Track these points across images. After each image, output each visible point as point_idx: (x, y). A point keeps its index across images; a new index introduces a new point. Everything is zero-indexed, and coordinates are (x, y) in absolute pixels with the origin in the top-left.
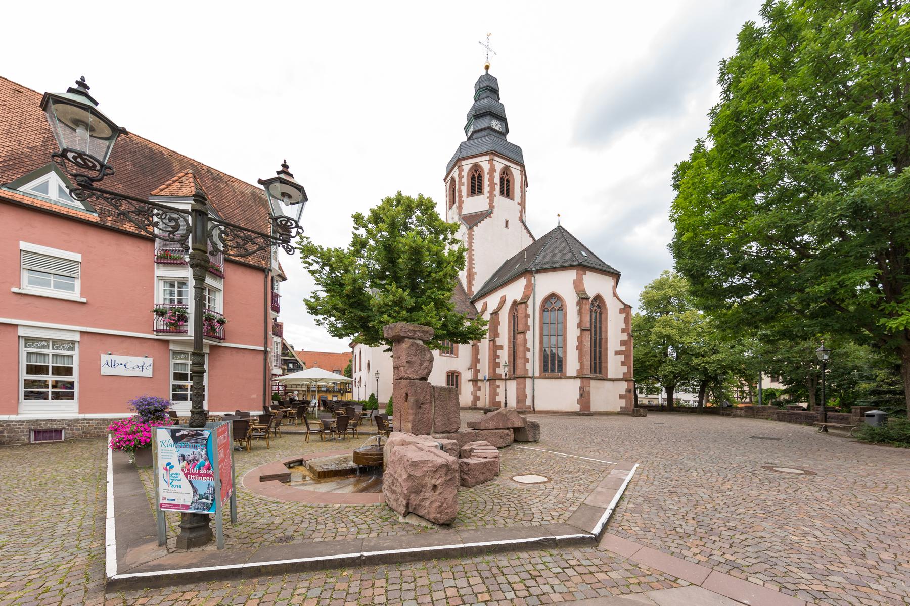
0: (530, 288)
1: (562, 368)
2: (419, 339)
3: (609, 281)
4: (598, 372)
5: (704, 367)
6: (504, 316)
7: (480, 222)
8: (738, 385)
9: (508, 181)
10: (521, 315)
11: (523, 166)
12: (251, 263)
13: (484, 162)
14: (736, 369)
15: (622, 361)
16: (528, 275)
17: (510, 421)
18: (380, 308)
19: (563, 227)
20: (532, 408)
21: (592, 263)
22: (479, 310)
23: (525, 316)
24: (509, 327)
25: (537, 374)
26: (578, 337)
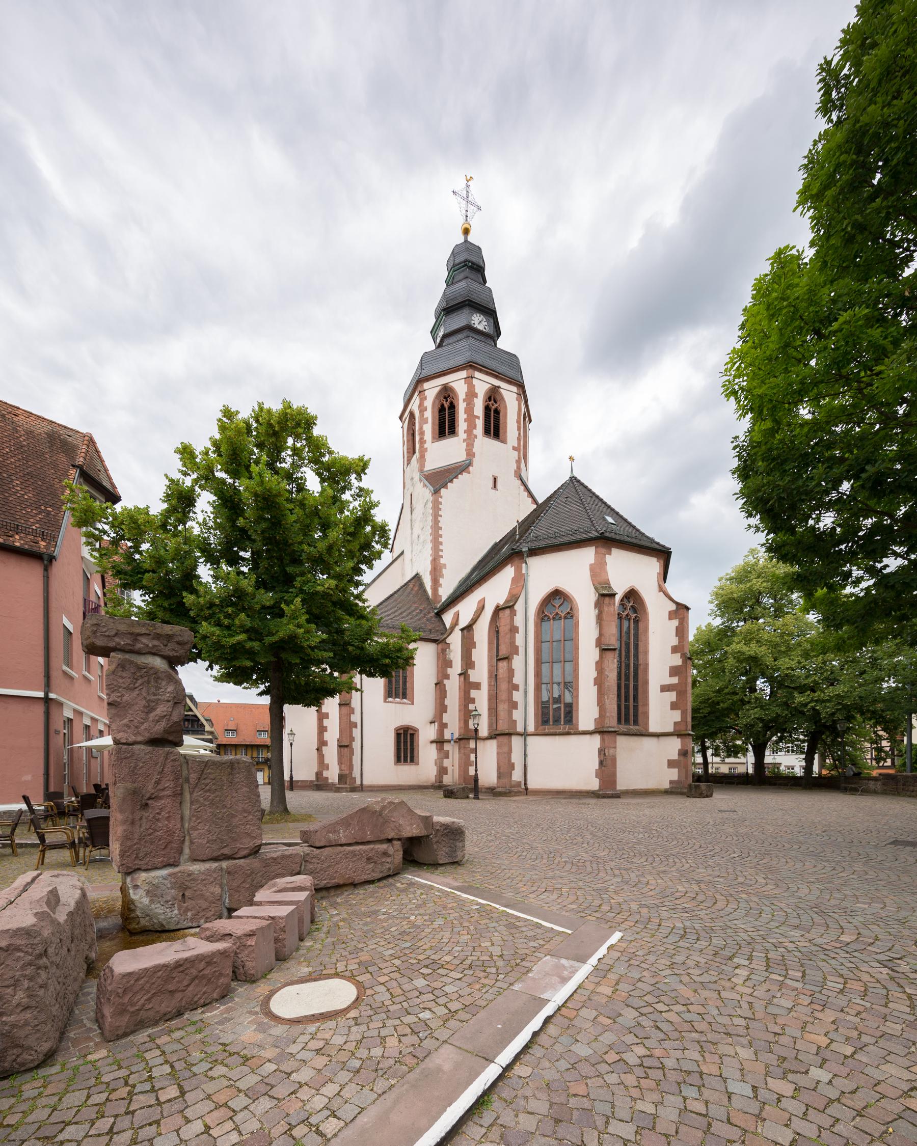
0: (520, 581)
1: (572, 717)
2: (154, 654)
3: (653, 565)
4: (632, 722)
5: (813, 708)
6: (482, 632)
7: (451, 481)
8: (871, 739)
9: (497, 412)
10: (504, 628)
11: (521, 386)
12: (17, 544)
13: (458, 382)
14: (868, 711)
15: (672, 703)
16: (517, 561)
17: (392, 825)
18: (202, 610)
19: (579, 478)
20: (523, 786)
21: (622, 532)
22: (448, 626)
23: (511, 630)
24: (490, 650)
25: (531, 728)
26: (597, 663)
